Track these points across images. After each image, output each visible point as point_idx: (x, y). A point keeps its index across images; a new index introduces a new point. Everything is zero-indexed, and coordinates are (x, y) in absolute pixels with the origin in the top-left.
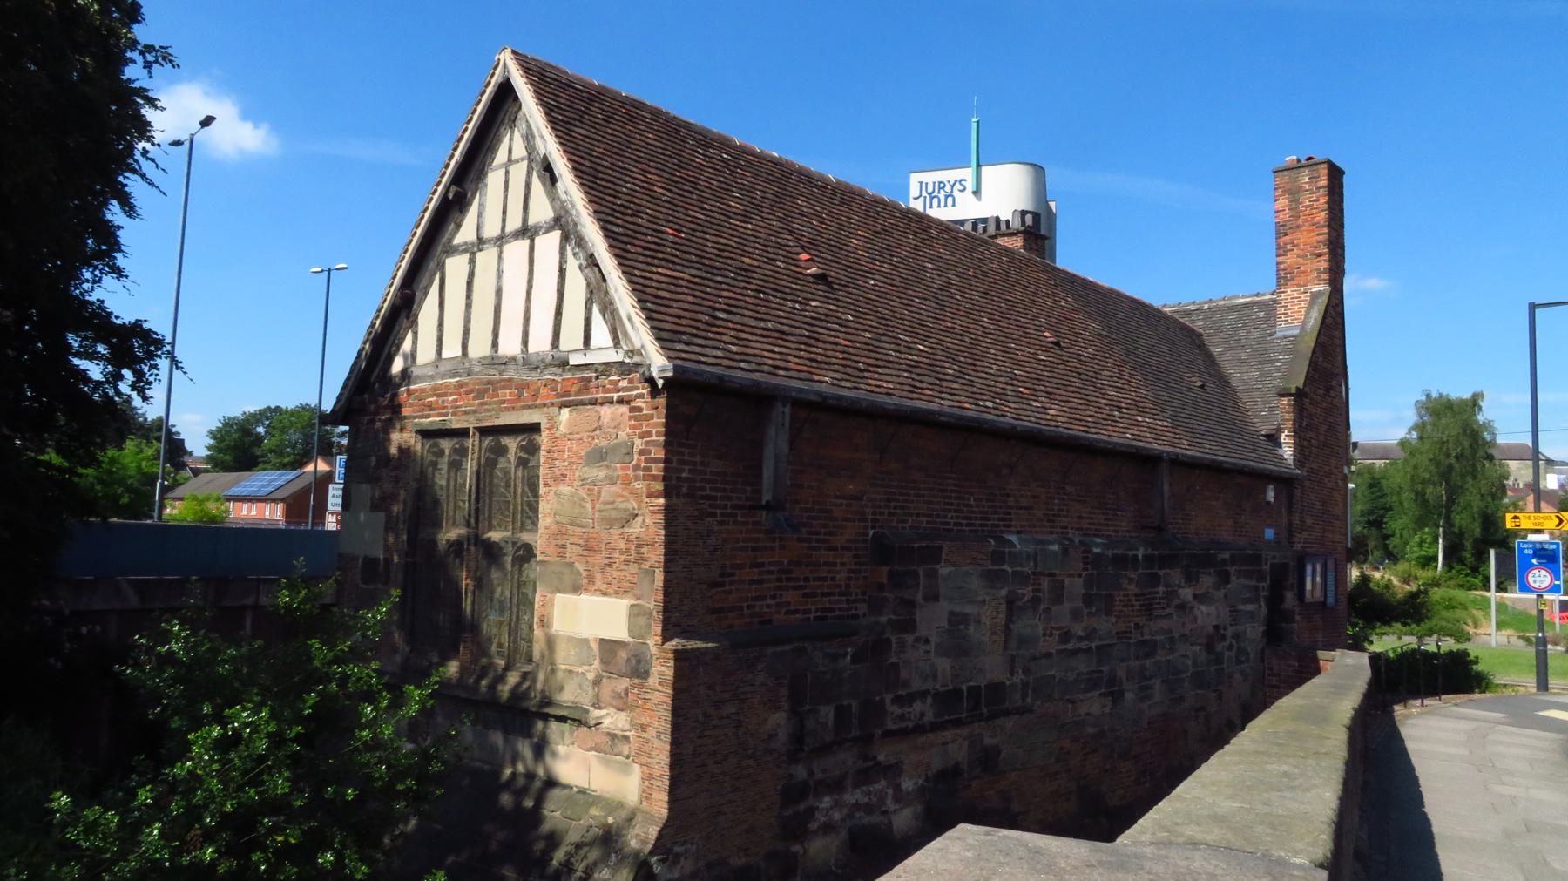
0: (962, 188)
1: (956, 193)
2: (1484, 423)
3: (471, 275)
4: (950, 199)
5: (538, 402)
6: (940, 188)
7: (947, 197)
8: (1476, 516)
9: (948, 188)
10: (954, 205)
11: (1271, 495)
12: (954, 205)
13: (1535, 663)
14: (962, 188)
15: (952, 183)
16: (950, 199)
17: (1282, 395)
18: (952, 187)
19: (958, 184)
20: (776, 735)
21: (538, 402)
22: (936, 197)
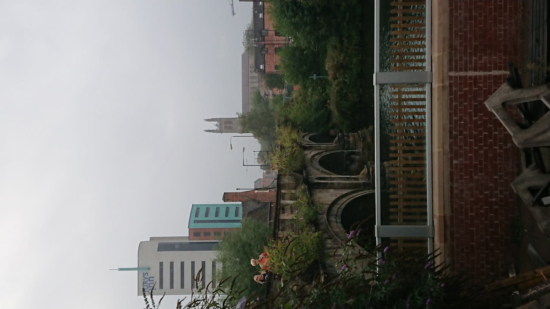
0: (147, 274)
1: (148, 277)
2: (283, 184)
3: (162, 298)
4: (151, 279)
5: (250, 73)
6: (146, 284)
7: (150, 281)
8: (320, 101)
9: (146, 280)
10: (153, 277)
11: (273, 205)
12: (153, 277)
13: (344, 194)
14: (147, 274)
15: (144, 278)
16: (151, 279)
17: (231, 276)
18: (145, 278)
19: (145, 276)
20: (294, 106)
21: (250, 73)
22: (149, 285)
